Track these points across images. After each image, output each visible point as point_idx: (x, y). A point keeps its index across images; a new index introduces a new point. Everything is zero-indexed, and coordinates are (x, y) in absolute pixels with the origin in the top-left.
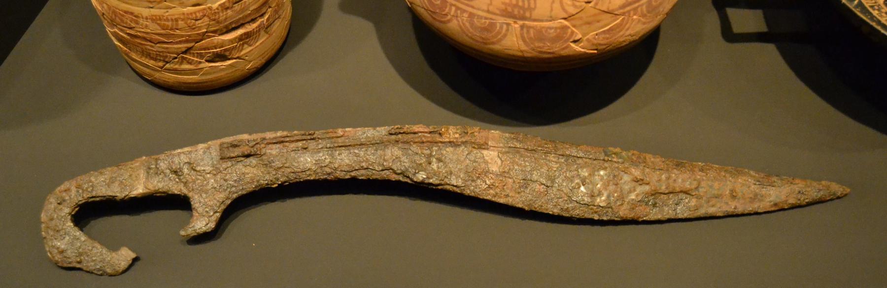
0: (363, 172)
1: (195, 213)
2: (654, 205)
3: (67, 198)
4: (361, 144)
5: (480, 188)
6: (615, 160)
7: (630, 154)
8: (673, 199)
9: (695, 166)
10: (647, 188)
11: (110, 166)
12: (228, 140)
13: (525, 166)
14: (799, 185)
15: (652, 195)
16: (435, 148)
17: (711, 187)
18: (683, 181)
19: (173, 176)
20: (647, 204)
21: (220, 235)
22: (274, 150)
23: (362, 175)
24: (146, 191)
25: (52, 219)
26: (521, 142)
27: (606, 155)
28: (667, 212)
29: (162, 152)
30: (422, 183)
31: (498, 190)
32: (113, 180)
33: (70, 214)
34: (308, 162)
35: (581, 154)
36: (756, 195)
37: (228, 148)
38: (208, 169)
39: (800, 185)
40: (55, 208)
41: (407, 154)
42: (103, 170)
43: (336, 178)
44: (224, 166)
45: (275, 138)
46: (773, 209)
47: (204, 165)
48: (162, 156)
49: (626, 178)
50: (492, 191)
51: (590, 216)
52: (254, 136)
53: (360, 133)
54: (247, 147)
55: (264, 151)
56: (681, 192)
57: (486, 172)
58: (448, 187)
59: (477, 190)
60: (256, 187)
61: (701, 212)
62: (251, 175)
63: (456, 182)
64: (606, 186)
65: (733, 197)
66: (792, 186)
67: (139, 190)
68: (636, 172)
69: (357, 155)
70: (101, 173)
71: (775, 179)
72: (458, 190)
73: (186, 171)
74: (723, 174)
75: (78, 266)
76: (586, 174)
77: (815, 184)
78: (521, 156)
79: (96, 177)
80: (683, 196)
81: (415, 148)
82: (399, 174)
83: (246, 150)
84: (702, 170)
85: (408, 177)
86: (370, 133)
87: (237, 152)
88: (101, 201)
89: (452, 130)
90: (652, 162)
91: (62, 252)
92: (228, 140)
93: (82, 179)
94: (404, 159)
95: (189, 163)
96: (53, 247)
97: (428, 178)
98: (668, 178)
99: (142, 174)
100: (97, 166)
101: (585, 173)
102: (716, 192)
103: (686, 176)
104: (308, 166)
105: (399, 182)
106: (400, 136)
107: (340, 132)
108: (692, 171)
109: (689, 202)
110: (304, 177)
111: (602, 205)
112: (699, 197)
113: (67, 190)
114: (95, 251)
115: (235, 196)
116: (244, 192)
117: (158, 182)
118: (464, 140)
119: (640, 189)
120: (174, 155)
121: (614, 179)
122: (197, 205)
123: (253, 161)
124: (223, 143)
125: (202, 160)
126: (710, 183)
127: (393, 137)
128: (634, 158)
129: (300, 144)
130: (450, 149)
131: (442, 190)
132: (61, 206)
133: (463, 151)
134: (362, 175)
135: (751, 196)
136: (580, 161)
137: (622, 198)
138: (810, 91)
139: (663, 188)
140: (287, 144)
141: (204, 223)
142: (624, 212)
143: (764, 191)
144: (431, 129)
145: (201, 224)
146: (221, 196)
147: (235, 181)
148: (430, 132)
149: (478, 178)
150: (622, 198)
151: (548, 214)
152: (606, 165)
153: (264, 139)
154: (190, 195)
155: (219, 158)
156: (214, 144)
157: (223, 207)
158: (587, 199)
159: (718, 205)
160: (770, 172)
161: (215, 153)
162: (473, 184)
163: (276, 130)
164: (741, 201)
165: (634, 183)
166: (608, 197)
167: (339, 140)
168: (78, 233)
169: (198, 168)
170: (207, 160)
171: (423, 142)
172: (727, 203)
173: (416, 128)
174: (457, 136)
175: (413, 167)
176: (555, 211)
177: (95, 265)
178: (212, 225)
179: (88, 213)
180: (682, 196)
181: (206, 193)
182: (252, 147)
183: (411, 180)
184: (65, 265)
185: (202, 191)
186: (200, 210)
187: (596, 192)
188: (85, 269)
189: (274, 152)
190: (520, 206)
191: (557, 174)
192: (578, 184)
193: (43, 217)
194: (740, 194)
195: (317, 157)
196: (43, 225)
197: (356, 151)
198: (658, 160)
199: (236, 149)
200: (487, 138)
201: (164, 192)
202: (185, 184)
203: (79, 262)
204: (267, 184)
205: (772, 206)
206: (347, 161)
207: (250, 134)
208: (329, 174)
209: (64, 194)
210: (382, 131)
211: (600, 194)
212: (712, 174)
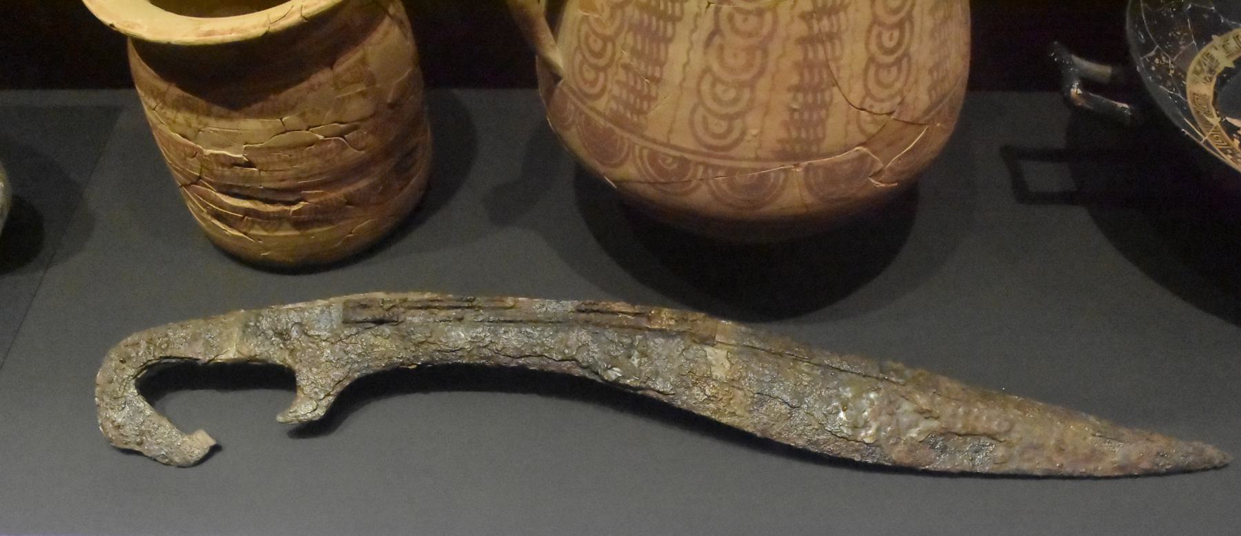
0: (535, 360)
1: (299, 393)
2: (944, 450)
3: (133, 355)
5: (696, 399)
10: (934, 424)
14: (1159, 443)
15: (942, 434)
18: (989, 419)
20: (933, 447)
22: (416, 318)
23: (534, 365)
25: (111, 382)
26: (763, 340)
27: (882, 372)
28: (962, 462)
30: (615, 383)
32: (195, 338)
33: (135, 377)
34: (460, 338)
36: (1094, 451)
41: (600, 344)
47: (319, 329)
48: (265, 312)
49: (906, 406)
50: (712, 405)
51: (849, 456)
61: (1011, 467)
62: (383, 348)
63: (661, 386)
64: (876, 415)
66: (1149, 444)
67: (230, 353)
68: (922, 401)
69: (529, 336)
72: (665, 399)
73: (294, 334)
74: (1049, 415)
75: (137, 448)
76: (850, 395)
81: (611, 334)
83: (377, 313)
86: (553, 307)
89: (666, 313)
90: (947, 389)
93: (157, 333)
95: (300, 324)
98: (967, 414)
99: (236, 333)
100: (181, 315)
101: (848, 393)
103: (996, 411)
104: (460, 343)
106: (592, 315)
107: (510, 301)
108: (1004, 406)
110: (453, 358)
111: (867, 440)
112: (1009, 445)
114: (162, 430)
115: (356, 375)
117: (256, 345)
119: (925, 425)
121: (890, 406)
122: (304, 383)
123: (387, 329)
127: (583, 316)
129: (453, 313)
130: (660, 341)
134: (533, 364)
137: (897, 434)
139: (960, 426)
140: (436, 311)
141: (311, 408)
142: (898, 454)
143: (1106, 447)
144: (637, 309)
146: (338, 374)
147: (359, 355)
148: (635, 314)
149: (695, 384)
150: (897, 434)
154: (296, 367)
155: (340, 321)
156: (337, 303)
157: (339, 389)
161: (336, 313)
163: (422, 290)
165: (917, 416)
166: (878, 430)
168: (142, 404)
169: (311, 333)
178: (321, 412)
179: (162, 381)
182: (388, 310)
185: (314, 363)
186: (307, 390)
187: (861, 423)
189: (416, 320)
190: (750, 429)
191: (808, 390)
192: (836, 407)
193: (99, 376)
196: (98, 389)
198: (955, 386)
200: (715, 330)
201: (262, 361)
202: (292, 352)
204: (402, 364)
205: (1115, 469)
206: (515, 343)
207: (388, 291)
208: (488, 358)
210: (569, 305)
211: (866, 425)
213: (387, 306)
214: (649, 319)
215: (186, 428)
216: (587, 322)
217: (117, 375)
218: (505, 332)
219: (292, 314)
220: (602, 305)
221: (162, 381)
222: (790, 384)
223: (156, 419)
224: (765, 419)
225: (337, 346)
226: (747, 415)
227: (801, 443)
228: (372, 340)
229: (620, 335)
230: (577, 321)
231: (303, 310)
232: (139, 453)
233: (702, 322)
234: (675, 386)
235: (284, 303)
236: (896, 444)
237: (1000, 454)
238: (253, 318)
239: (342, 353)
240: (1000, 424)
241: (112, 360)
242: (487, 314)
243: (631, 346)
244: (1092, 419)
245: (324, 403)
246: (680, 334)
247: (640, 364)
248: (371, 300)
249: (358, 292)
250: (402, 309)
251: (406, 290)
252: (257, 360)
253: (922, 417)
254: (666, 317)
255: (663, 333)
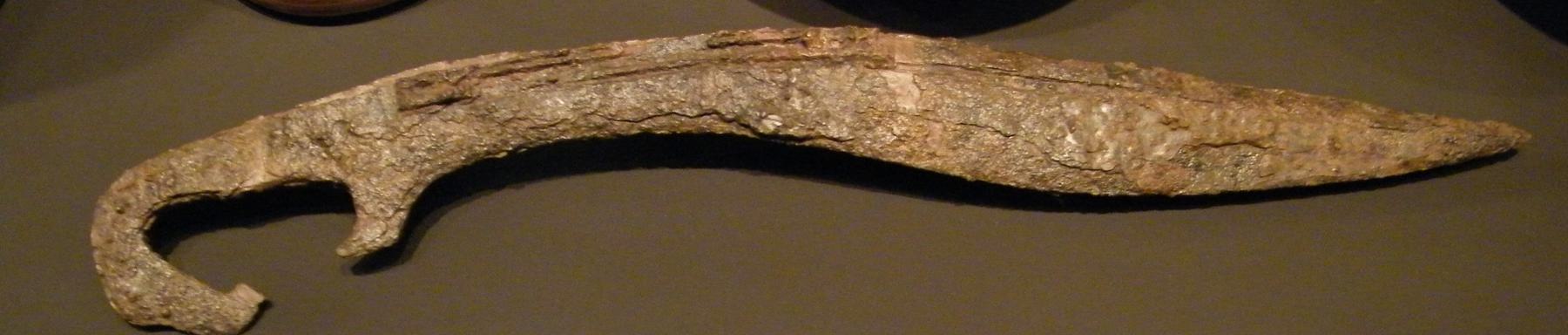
0: (663, 120)
1: (361, 215)
2: (1198, 167)
3: (132, 200)
4: (659, 69)
5: (883, 142)
6: (1126, 84)
7: (1153, 74)
8: (1228, 157)
9: (1268, 96)
10: (1185, 136)
11: (203, 137)
12: (415, 72)
13: (965, 99)
14: (1447, 127)
15: (1195, 148)
16: (795, 70)
17: (1297, 132)
18: (1249, 121)
19: (314, 148)
20: (1184, 165)
21: (411, 253)
22: (495, 89)
23: (662, 127)
24: (269, 179)
25: (110, 241)
26: (954, 54)
27: (1110, 76)
28: (1219, 181)
29: (292, 106)
30: (774, 136)
31: (915, 145)
32: (209, 163)
33: (140, 229)
34: (562, 106)
35: (1066, 76)
36: (1373, 147)
37: (410, 88)
38: (379, 130)
39: (1449, 129)
40: (114, 221)
41: (743, 84)
42: (191, 145)
43: (614, 134)
44: (407, 122)
45: (497, 65)
46: (1402, 172)
47: (369, 124)
48: (293, 113)
49: (1148, 118)
50: (903, 148)
51: (1084, 190)
52: (459, 64)
53: (654, 47)
54: (445, 86)
55: (477, 89)
56: (1245, 142)
57: (894, 113)
58: (823, 142)
59: (877, 146)
60: (468, 158)
61: (1280, 180)
62: (457, 136)
63: (837, 131)
64: (1111, 135)
65: (1335, 150)
66: (1435, 130)
67: (257, 178)
68: (1166, 107)
69: (650, 90)
70: (187, 151)
71: (1404, 117)
72: (841, 148)
73: (338, 136)
74: (1317, 108)
75: (166, 322)
76: (1077, 112)
77: (1472, 126)
78: (957, 81)
79: (179, 158)
80: (1250, 150)
81: (758, 71)
82: (730, 121)
83: (445, 90)
84: (1280, 103)
85: (747, 126)
86: (673, 46)
87: (428, 95)
88: (193, 203)
89: (826, 34)
90: (1194, 89)
91: (135, 299)
92: (415, 72)
93: (156, 165)
94: (738, 92)
95: (342, 122)
96: (119, 291)
97: (785, 126)
98: (1223, 117)
99: (261, 150)
100: (181, 138)
101: (1074, 110)
102: (1305, 142)
103: (1254, 112)
104: (561, 114)
105: (729, 137)
106: (728, 50)
107: (616, 47)
108: (1263, 104)
109: (1259, 160)
110: (554, 136)
111: (1106, 167)
112: (1276, 152)
113: (131, 187)
114: (191, 293)
115: (430, 178)
116: (447, 170)
117: (292, 160)
118: (849, 52)
119: (1174, 138)
120: (314, 109)
121: (1128, 121)
122: (363, 199)
123: (459, 110)
124: (402, 81)
125: (367, 114)
126: (1295, 125)
127: (716, 52)
128: (1161, 81)
129: (543, 74)
130: (824, 71)
131: (811, 148)
132: (124, 216)
133: (847, 74)
134: (661, 126)
135: (1366, 148)
136: (1063, 88)
137: (1140, 155)
138: (1122, 215)
139: (1214, 135)
140: (519, 75)
141: (379, 231)
142: (1145, 180)
143: (1386, 140)
144: (786, 33)
145: (374, 232)
146: (405, 180)
147: (429, 150)
148: (786, 41)
149: (878, 123)
150: (1140, 155)
151: (1009, 187)
152: (1112, 94)
153: (475, 68)
154: (349, 180)
155: (396, 108)
156: (386, 85)
157: (411, 200)
158: (1078, 159)
159: (1308, 166)
160: (1395, 111)
161: (388, 99)
162: (870, 135)
163: (496, 50)
164: (1348, 158)
165: (1163, 128)
166: (1117, 152)
167: (616, 63)
168: (160, 264)
169: (360, 131)
170: (374, 115)
171: (773, 60)
172: (1324, 162)
173: (758, 34)
174: (836, 45)
175: (756, 108)
176: (1021, 180)
177: (196, 318)
178: (394, 235)
179: (174, 226)
180: (1243, 149)
181: (378, 176)
182: (456, 84)
183: (754, 130)
184: (144, 323)
185: (371, 171)
186: (370, 208)
187: (1095, 146)
188: (178, 327)
189: (496, 92)
190: (956, 172)
191: (1023, 111)
192: (1061, 129)
193: (95, 238)
194: (1347, 145)
195: (576, 96)
196: (97, 254)
197: (649, 82)
198: (1202, 86)
199: (426, 90)
200: (892, 49)
201: (303, 180)
202: (340, 161)
203: (167, 316)
204: (488, 153)
205: (1400, 167)
206: (632, 102)
207: (450, 60)
208: (599, 128)
209: (126, 194)
210: (697, 41)
211: (1102, 148)
212: (1297, 110)
213: (455, 78)
214: (804, 44)
215: (224, 286)
216: (724, 60)
217: (118, 225)
218: (617, 89)
219: (330, 110)
220: (738, 35)
221: (174, 226)
222: (999, 106)
223: (180, 278)
224: (975, 156)
225: (398, 144)
226: (951, 154)
227: (1022, 181)
228: (443, 128)
229: (772, 72)
230: (709, 61)
231: (343, 102)
232: (170, 328)
233: (876, 40)
234: (853, 129)
235: (315, 97)
236: (1140, 167)
237: (1266, 164)
238: (278, 125)
239: (405, 151)
240: (1262, 127)
241: (105, 212)
242: (588, 69)
243: (788, 84)
244: (1366, 107)
245: (395, 222)
246: (850, 59)
247: (804, 106)
248: (432, 74)
249: (410, 68)
250: (475, 80)
251: (475, 55)
252: (295, 180)
253: (1166, 128)
254: (827, 39)
255: (825, 60)
